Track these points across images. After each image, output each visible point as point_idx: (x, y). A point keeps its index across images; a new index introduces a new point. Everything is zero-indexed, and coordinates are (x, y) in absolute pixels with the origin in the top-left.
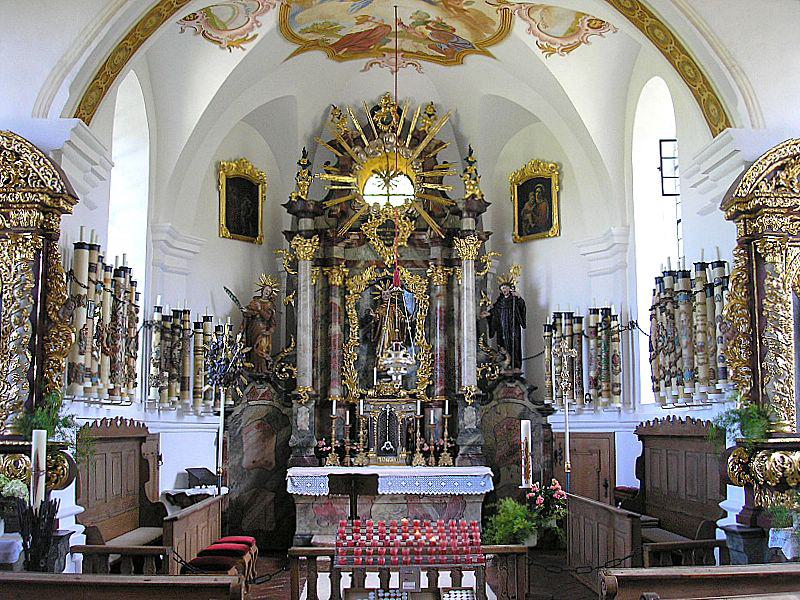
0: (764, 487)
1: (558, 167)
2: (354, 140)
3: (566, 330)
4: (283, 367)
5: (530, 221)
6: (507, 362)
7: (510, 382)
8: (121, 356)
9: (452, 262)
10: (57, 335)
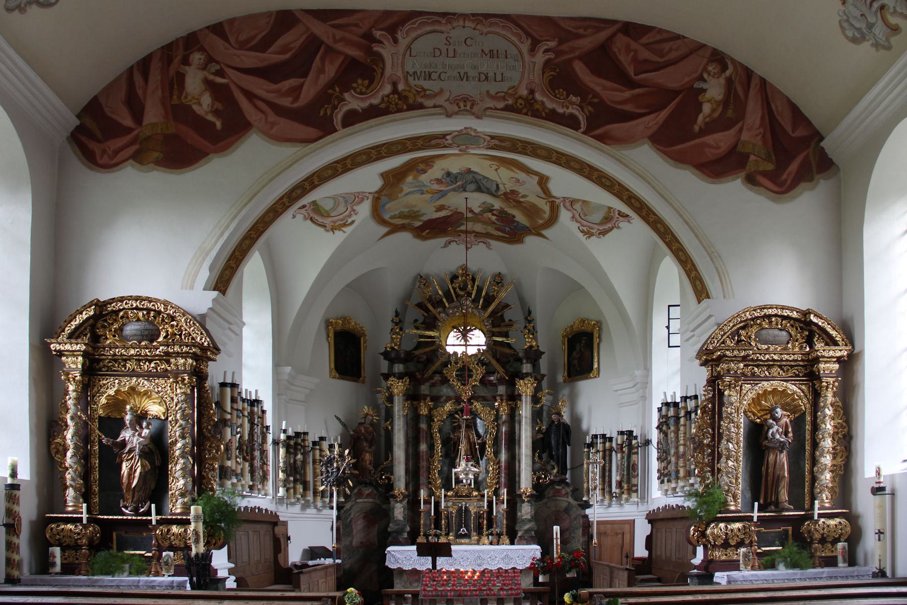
1: (599, 324)
2: (437, 302)
3: (600, 447)
4: (383, 475)
6: (555, 471)
7: (558, 485)
8: (257, 463)
9: (514, 398)
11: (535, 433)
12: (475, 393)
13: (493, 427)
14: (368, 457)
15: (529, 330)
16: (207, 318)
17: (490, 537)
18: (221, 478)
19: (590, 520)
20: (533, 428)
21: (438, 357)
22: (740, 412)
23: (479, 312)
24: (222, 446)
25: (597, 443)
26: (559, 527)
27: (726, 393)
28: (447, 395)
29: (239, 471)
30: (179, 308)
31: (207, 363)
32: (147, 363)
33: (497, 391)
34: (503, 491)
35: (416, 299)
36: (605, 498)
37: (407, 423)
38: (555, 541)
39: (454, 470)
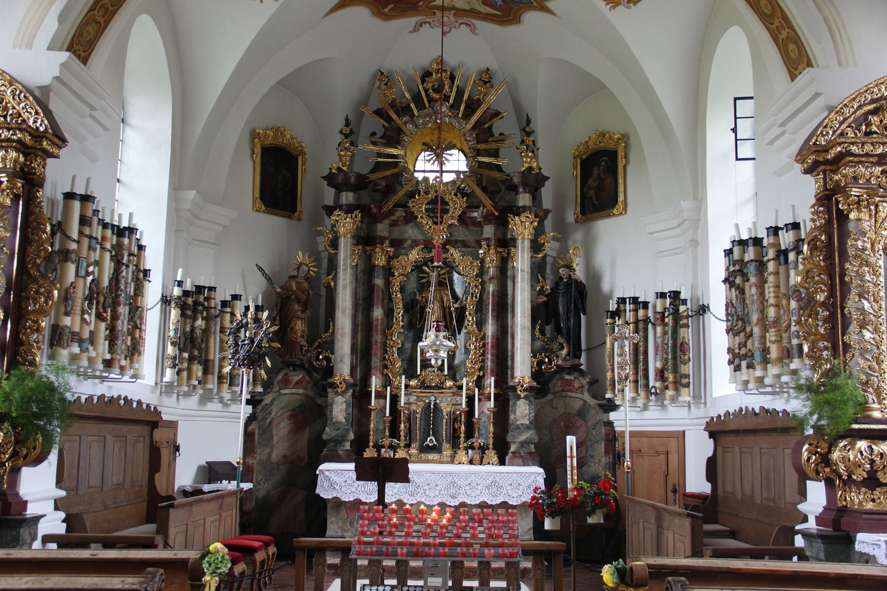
0: (849, 482)
1: (625, 138)
2: (403, 108)
3: (630, 316)
4: (320, 353)
5: (594, 198)
6: (564, 352)
7: (569, 374)
8: (123, 325)
9: (506, 243)
10: (37, 292)
11: (536, 293)
12: (452, 235)
13: (476, 286)
14: (299, 326)
15: (527, 146)
16: (51, 94)
17: (470, 451)
18: (52, 345)
19: (616, 429)
20: (533, 287)
21: (402, 185)
22: (876, 249)
23: (459, 123)
24: (56, 292)
25: (625, 311)
26: (574, 438)
27: (852, 216)
28: (413, 238)
29: (86, 335)
30: (3, 72)
31: (44, 160)
33: (482, 234)
34: (489, 381)
35: (375, 104)
36: (639, 395)
37: (356, 278)
38: (569, 460)
39: (420, 344)
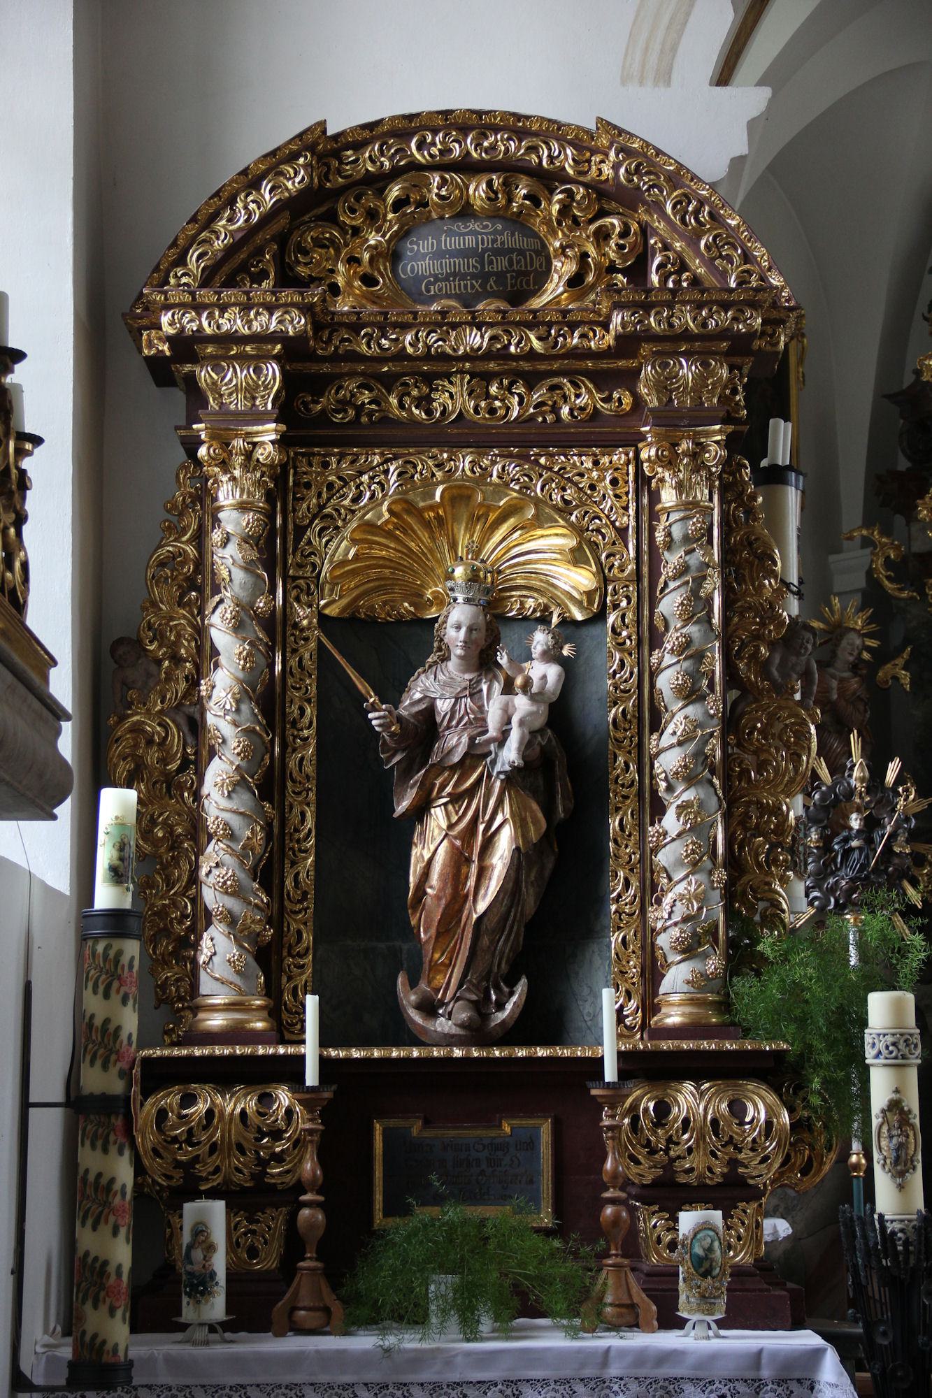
32: (520, 389)
